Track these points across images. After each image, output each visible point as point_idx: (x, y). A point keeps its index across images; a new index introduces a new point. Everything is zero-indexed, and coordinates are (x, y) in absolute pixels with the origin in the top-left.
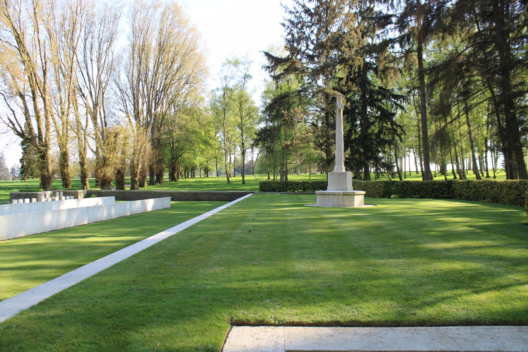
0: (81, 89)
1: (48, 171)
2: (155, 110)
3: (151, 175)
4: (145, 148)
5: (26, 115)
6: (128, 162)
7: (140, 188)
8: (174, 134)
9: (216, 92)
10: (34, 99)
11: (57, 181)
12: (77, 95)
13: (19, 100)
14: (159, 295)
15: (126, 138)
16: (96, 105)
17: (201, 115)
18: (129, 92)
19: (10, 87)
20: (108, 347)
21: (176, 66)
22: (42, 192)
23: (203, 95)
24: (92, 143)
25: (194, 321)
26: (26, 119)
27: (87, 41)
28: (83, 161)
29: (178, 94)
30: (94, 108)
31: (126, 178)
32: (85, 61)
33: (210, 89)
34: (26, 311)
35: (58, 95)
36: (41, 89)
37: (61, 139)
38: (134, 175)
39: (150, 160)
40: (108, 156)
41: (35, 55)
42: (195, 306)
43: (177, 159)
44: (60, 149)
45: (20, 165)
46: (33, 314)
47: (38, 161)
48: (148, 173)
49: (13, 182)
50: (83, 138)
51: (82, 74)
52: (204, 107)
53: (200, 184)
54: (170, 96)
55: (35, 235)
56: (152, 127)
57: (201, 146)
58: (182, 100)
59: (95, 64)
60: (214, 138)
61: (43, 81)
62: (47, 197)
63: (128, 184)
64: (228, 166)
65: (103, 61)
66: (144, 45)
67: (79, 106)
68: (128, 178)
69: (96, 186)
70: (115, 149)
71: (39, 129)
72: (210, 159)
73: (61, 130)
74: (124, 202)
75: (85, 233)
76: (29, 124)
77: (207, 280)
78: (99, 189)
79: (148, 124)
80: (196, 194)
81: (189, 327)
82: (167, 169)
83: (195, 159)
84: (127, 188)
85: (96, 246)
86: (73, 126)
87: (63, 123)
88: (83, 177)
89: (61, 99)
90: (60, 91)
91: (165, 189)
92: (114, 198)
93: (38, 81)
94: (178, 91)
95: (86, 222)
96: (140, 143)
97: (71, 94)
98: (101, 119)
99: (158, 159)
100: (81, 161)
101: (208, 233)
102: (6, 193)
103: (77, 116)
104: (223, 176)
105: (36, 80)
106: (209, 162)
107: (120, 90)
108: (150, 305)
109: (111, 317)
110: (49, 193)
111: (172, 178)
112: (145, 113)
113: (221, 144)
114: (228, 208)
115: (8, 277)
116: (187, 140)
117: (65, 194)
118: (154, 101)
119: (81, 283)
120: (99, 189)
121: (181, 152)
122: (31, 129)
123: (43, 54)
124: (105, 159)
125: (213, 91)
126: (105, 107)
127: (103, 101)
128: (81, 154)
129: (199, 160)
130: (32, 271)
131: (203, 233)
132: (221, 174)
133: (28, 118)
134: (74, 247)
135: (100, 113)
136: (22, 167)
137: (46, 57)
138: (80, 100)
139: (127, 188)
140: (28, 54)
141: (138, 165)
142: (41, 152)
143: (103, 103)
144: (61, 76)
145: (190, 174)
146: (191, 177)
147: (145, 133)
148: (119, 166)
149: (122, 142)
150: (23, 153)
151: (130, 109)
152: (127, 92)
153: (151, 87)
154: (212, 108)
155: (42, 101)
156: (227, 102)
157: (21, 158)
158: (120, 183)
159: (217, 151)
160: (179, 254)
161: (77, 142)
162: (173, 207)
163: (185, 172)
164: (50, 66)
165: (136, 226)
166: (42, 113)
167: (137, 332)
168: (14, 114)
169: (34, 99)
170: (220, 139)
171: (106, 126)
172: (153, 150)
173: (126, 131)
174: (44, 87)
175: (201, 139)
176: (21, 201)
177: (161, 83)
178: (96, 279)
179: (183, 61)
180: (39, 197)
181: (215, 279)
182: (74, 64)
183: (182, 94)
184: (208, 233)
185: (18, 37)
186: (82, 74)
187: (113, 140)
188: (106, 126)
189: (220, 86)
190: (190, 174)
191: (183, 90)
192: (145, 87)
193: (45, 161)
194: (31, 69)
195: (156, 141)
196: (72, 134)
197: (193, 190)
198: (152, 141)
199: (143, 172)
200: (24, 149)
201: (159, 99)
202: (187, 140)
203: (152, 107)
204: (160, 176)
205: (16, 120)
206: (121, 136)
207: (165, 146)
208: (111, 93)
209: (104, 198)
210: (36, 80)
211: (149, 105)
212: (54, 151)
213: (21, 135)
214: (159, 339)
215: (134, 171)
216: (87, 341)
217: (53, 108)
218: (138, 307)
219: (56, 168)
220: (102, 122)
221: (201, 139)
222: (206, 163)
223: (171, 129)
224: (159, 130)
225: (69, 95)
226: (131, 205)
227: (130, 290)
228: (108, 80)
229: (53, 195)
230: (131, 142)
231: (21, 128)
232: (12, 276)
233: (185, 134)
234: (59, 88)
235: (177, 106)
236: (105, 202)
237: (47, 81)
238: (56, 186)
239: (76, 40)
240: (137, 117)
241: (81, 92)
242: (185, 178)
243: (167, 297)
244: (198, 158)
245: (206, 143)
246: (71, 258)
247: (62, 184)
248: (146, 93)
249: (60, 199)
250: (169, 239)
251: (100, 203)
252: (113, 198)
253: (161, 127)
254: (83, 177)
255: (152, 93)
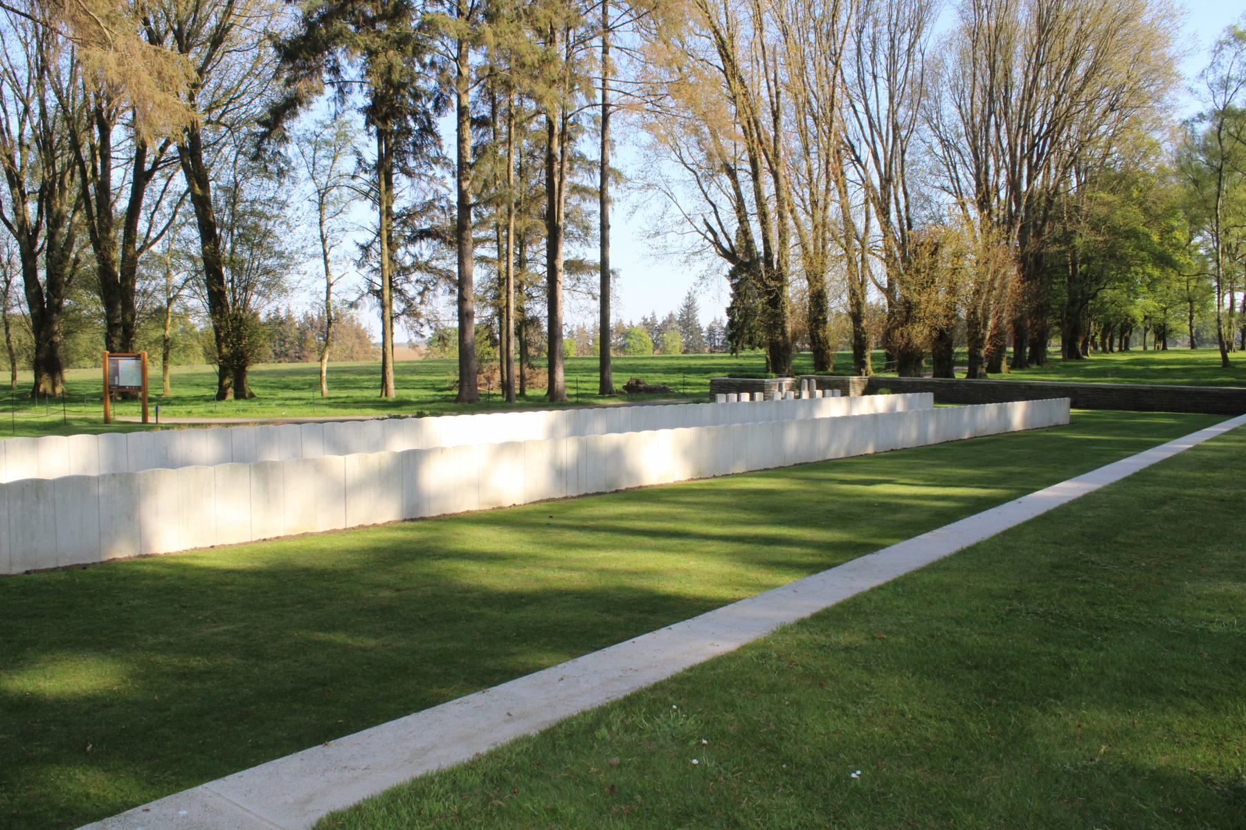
0: (853, 148)
1: (783, 333)
2: (1029, 183)
3: (1019, 347)
4: (1004, 278)
5: (738, 212)
6: (963, 313)
7: (989, 375)
8: (1078, 241)
9: (1196, 125)
10: (755, 176)
11: (802, 357)
12: (846, 161)
13: (726, 180)
14: (1085, 632)
15: (958, 255)
16: (886, 180)
17: (1149, 188)
18: (964, 144)
19: (710, 156)
20: (981, 734)
21: (1080, 71)
22: (772, 380)
23: (1156, 136)
24: (879, 269)
25: (1189, 709)
26: (741, 222)
27: (864, 34)
28: (859, 312)
29: (1089, 139)
30: (883, 188)
31: (957, 350)
32: (861, 79)
33: (1178, 116)
34: (792, 627)
35: (804, 165)
36: (770, 154)
37: (811, 263)
38: (975, 342)
39: (1016, 308)
40: (915, 298)
41: (756, 79)
42: (1187, 671)
43: (1084, 302)
44: (810, 284)
45: (726, 320)
46: (805, 636)
47: (764, 311)
48: (1009, 337)
49: (712, 358)
50: (859, 258)
51: (855, 112)
52: (1160, 168)
53: (1144, 369)
54: (1068, 146)
55: (765, 472)
56: (1022, 227)
57: (1149, 269)
58: (1098, 154)
59: (883, 84)
60: (1187, 249)
61: (772, 134)
62: (784, 390)
63: (962, 364)
64: (1225, 321)
65: (900, 76)
66: (999, 28)
67: (849, 184)
68: (961, 350)
69: (888, 368)
70: (933, 282)
71: (766, 241)
72: (1172, 304)
73: (811, 242)
74: (955, 406)
75: (870, 472)
76: (744, 232)
77: (1209, 611)
78: (893, 375)
79: (1010, 220)
80: (1135, 392)
81: (1179, 722)
82: (1057, 328)
83: (1132, 303)
84: (960, 375)
85: (896, 504)
86: (837, 232)
87: (816, 227)
88: (859, 345)
89: (810, 172)
90: (808, 154)
91: (1053, 379)
92: (930, 396)
93: (762, 137)
94: (1088, 130)
95: (870, 450)
96: (991, 267)
97: (831, 160)
98: (899, 211)
99: (1035, 304)
100: (855, 310)
101: (1190, 492)
102: (700, 381)
103: (845, 208)
104: (1208, 347)
105: (759, 135)
106: (1169, 311)
107: (942, 141)
108: (1065, 652)
109: (976, 667)
110: (788, 381)
111: (1071, 351)
112: (1002, 194)
113: (1204, 265)
114: (1234, 431)
115: (720, 555)
116: (1111, 254)
117: (822, 385)
118: (1026, 161)
119: (895, 583)
120: (893, 375)
121: (1094, 288)
122: (750, 243)
123: (772, 76)
124: (909, 306)
125: (1185, 122)
126: (908, 183)
127: (902, 170)
128: (853, 294)
129: (1142, 306)
130: (766, 548)
131: (1177, 490)
132: (1202, 342)
133: (743, 220)
134: (849, 503)
135: (896, 199)
136: (731, 324)
137: (779, 82)
138: (852, 173)
139: (960, 375)
140: (742, 81)
141: (986, 318)
142: (769, 293)
143: (903, 176)
144: (810, 121)
145: (1117, 341)
146: (1120, 350)
147: (1003, 242)
148: (942, 322)
149: (949, 265)
150: (732, 296)
151: (966, 184)
152: (960, 146)
153: (1019, 127)
154: (1182, 169)
155: (772, 180)
156: (1227, 148)
157: (729, 305)
158: (944, 363)
159: (1193, 283)
160: (1121, 539)
161: (845, 267)
162: (1074, 424)
163: (1103, 337)
164: (786, 99)
165: (988, 464)
166: (771, 206)
167: (1044, 710)
168: (716, 212)
169: (755, 176)
170: (1202, 251)
171: (910, 227)
172: (1023, 282)
173: (958, 238)
174: (775, 149)
175: (1152, 253)
176: (734, 397)
177: (1045, 114)
178: (927, 579)
179: (1101, 52)
180: (767, 390)
181: (1231, 611)
182: (838, 90)
183: (1100, 137)
184: (1190, 492)
185: (722, 47)
186: (855, 112)
187: (927, 260)
188: (910, 227)
189: (1206, 107)
190: (1117, 341)
191: (1103, 129)
192: (1004, 127)
193: (779, 311)
194: (748, 110)
195: (1030, 259)
196: (834, 250)
197: (1126, 383)
198: (1022, 260)
199: (998, 334)
200: (735, 287)
201: (1039, 156)
202: (1112, 256)
203: (1021, 177)
204: (1039, 347)
205: (720, 224)
206: (947, 251)
207: (1055, 271)
208: (923, 148)
209: (909, 395)
210: (759, 135)
211: (1013, 172)
212: (796, 289)
213: (729, 255)
214: (1101, 738)
215: (977, 333)
216: (930, 711)
217: (794, 193)
218: (1037, 654)
219: (800, 327)
220: (900, 221)
221: (1152, 253)
222: (1160, 315)
223: (1069, 228)
224: (1039, 233)
225: (828, 162)
226: (973, 415)
227: (1011, 611)
228: (913, 120)
229: (797, 387)
230: (969, 262)
231: (729, 240)
232: (728, 554)
233: (1106, 241)
234: (806, 149)
235: (1086, 171)
236: (909, 405)
237: (781, 135)
238: (800, 367)
239: (841, 36)
240: (983, 203)
241: (854, 152)
242: (1104, 351)
243: (1106, 639)
244: (1139, 301)
245: (1163, 261)
246: (844, 528)
247: (811, 362)
248: (1005, 143)
249: (812, 395)
250: (1086, 501)
251: (900, 408)
252: (929, 396)
253: (1043, 224)
254: (859, 345)
255: (1023, 143)
